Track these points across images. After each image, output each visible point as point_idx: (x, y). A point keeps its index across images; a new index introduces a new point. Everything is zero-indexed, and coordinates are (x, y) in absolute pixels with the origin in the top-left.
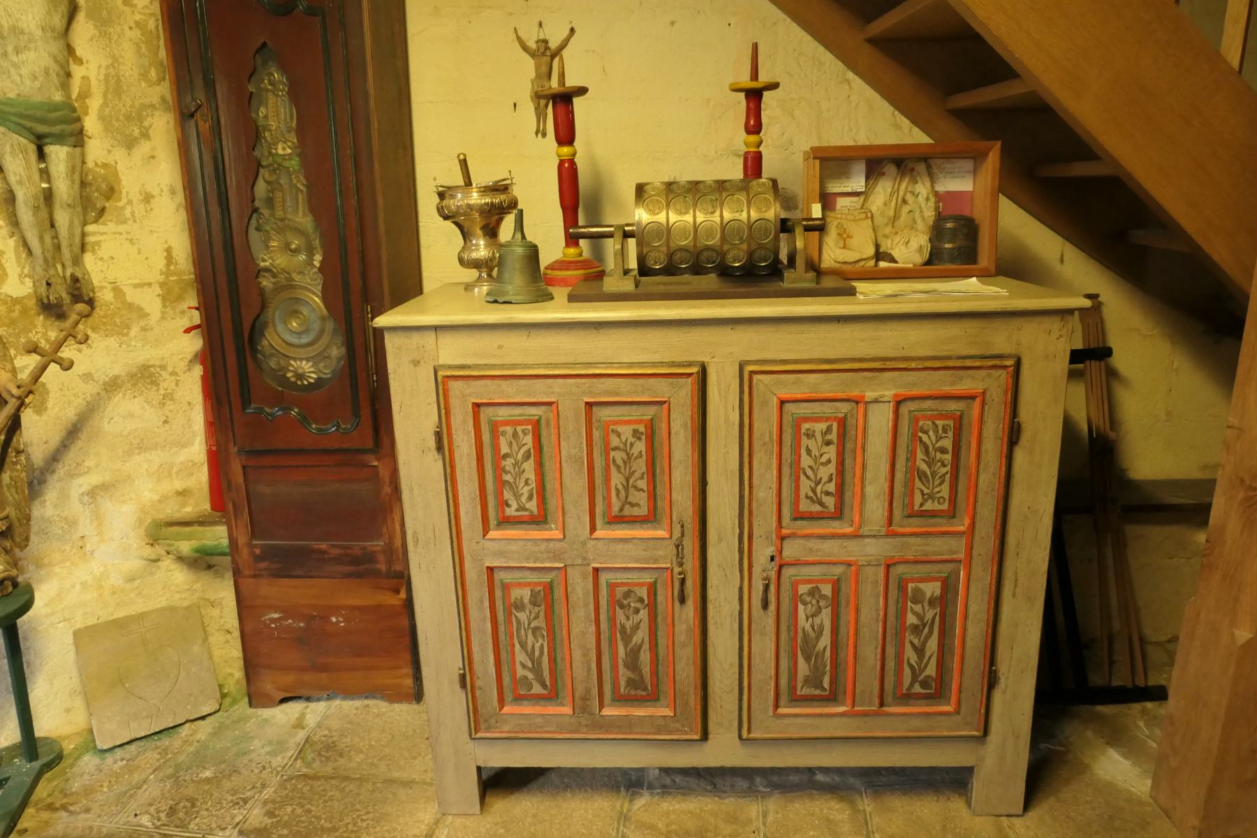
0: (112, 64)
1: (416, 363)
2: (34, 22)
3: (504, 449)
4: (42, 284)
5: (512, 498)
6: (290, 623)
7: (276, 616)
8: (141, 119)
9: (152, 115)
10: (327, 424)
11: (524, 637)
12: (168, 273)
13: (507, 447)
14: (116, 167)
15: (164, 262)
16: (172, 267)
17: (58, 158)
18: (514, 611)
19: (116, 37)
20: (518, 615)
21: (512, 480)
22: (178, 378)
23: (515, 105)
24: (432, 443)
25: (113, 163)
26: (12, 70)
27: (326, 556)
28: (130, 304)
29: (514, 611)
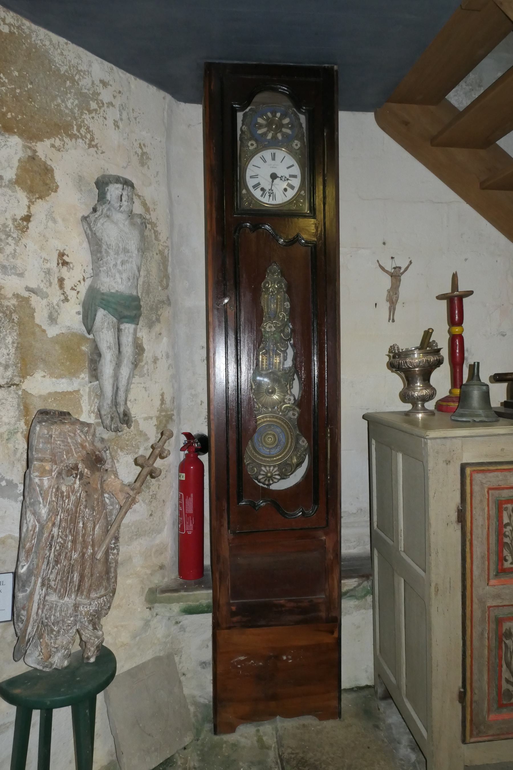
0: (146, 275)
1: (448, 462)
2: (134, 245)
3: (506, 520)
4: (108, 418)
5: (509, 555)
6: (252, 663)
7: (242, 658)
8: (157, 309)
9: (163, 307)
10: (294, 511)
11: (509, 659)
12: (161, 410)
13: (508, 518)
14: (142, 340)
15: (159, 402)
16: (163, 406)
17: (129, 332)
18: (504, 639)
19: (150, 259)
20: (507, 642)
21: (509, 542)
22: (160, 483)
23: (376, 304)
24: (454, 516)
25: (141, 337)
26: (117, 275)
27: (283, 609)
28: (141, 431)
29: (504, 639)
